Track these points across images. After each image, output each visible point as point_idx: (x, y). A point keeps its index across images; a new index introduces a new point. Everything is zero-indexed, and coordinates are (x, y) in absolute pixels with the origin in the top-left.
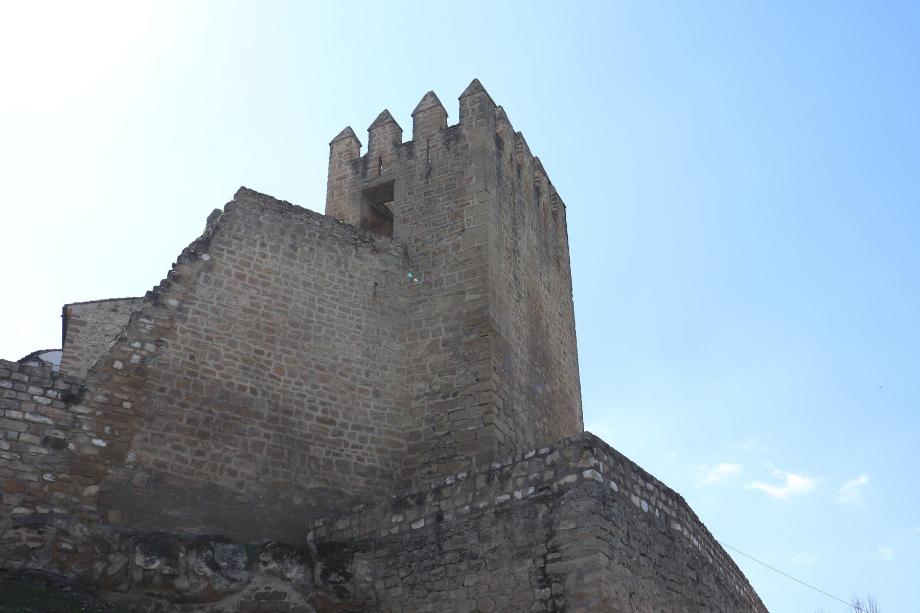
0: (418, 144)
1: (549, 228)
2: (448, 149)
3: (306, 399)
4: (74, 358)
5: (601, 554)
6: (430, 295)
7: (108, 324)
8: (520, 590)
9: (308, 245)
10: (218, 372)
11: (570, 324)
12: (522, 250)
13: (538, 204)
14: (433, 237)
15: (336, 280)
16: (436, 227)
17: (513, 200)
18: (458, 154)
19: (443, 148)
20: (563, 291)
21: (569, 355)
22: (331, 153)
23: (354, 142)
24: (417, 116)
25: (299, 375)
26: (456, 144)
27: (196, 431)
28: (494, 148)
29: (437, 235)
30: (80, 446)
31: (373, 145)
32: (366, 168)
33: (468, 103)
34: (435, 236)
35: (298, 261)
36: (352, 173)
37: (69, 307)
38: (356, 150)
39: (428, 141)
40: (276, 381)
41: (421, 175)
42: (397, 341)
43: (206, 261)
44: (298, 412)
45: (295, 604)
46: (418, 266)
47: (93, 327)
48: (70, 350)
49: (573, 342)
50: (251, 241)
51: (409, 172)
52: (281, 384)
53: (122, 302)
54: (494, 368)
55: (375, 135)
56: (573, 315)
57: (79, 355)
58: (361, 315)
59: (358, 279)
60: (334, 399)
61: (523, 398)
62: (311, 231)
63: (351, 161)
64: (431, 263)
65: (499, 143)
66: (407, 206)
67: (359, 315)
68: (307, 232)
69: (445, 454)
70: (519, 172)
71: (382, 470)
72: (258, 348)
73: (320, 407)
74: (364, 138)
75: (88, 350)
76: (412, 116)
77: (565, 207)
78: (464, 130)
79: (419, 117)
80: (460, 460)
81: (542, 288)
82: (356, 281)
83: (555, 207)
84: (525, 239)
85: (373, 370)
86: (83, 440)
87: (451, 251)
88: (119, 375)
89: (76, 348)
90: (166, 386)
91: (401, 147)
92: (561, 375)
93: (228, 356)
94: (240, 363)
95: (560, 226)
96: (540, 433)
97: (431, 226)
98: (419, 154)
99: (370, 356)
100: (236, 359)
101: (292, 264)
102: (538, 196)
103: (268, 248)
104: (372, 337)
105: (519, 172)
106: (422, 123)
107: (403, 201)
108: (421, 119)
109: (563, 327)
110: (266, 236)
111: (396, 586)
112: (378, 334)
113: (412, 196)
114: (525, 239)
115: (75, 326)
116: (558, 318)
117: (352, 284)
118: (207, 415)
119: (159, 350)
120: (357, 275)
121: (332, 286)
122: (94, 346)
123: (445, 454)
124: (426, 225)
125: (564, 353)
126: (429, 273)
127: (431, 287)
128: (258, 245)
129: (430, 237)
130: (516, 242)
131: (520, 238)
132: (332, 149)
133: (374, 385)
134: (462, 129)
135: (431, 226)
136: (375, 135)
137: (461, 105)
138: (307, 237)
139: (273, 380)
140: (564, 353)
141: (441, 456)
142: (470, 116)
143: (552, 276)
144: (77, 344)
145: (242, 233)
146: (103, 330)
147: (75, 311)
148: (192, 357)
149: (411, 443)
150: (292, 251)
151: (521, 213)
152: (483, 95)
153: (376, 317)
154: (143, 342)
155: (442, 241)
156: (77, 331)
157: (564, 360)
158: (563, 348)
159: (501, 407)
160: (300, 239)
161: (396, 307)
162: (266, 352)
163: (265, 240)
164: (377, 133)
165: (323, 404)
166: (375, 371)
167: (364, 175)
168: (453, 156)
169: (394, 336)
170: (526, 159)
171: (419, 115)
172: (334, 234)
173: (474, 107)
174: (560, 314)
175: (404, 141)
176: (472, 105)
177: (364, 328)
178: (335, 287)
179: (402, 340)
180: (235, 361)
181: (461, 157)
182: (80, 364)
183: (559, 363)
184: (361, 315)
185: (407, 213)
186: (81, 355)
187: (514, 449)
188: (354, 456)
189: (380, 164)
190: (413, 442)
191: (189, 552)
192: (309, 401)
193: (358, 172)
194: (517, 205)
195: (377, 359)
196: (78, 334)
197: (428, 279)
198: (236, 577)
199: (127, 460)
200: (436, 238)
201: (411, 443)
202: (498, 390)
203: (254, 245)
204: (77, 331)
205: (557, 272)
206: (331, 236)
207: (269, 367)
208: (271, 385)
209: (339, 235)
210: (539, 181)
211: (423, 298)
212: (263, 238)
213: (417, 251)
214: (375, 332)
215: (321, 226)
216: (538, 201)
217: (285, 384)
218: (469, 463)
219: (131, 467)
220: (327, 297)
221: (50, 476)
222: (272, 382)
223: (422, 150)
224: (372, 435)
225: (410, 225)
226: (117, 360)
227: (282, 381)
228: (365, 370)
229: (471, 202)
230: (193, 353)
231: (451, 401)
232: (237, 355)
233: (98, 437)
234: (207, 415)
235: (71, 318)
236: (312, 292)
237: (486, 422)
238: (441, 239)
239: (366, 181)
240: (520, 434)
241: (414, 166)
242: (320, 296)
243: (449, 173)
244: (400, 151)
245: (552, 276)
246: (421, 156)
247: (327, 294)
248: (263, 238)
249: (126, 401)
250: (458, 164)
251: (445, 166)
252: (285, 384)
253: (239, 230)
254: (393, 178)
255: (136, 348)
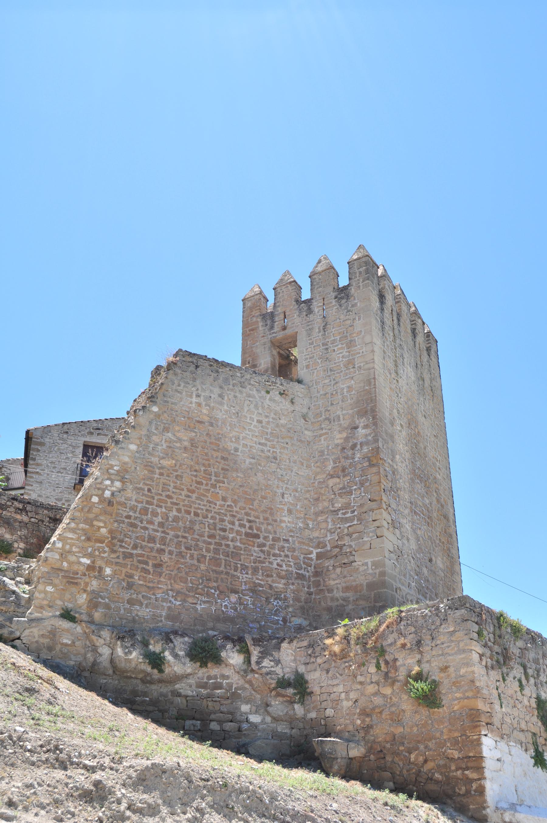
0: (316, 301)
1: (424, 364)
2: (340, 306)
3: (237, 518)
4: (37, 473)
5: (474, 652)
6: (330, 429)
7: (62, 444)
8: (338, 486)
9: (232, 393)
10: (169, 501)
11: (444, 443)
12: (402, 387)
13: (415, 344)
14: (330, 381)
15: (255, 420)
16: (332, 373)
17: (395, 346)
18: (349, 311)
19: (336, 306)
20: (437, 415)
21: (443, 470)
22: (244, 308)
23: (262, 299)
24: (314, 277)
25: (230, 500)
26: (346, 302)
27: (155, 548)
28: (378, 304)
29: (334, 380)
30: (70, 563)
31: (278, 302)
32: (273, 322)
33: (356, 267)
34: (332, 380)
35: (226, 407)
36: (262, 326)
37: (30, 431)
38: (264, 305)
39: (324, 299)
40: (213, 506)
41: (319, 328)
42: (305, 468)
43: (155, 412)
44: (232, 529)
45: (237, 684)
46: (319, 405)
47: (50, 447)
48: (33, 466)
49: (446, 458)
50: (189, 393)
51: (309, 325)
52: (217, 507)
53: (74, 425)
54: (384, 490)
55: (279, 293)
56: (446, 435)
57: (41, 470)
58: (276, 448)
59: (273, 418)
60: (258, 517)
61: (407, 511)
62: (234, 381)
63: (260, 315)
64: (330, 403)
65: (382, 298)
66: (308, 354)
67: (273, 448)
68: (231, 383)
69: (346, 560)
70: (399, 320)
71: (297, 573)
72: (198, 479)
73: (248, 525)
74: (270, 296)
75: (48, 466)
76: (310, 277)
77: (437, 342)
78: (353, 289)
79: (315, 278)
80: (359, 565)
81: (420, 416)
82: (271, 420)
83: (428, 343)
84: (404, 377)
85: (287, 492)
86: (73, 558)
87: (345, 393)
88: (96, 507)
89: (38, 465)
90: (131, 513)
91: (301, 304)
92: (437, 488)
93: (175, 487)
94: (184, 493)
95: (433, 359)
96: (421, 539)
97: (329, 371)
98: (316, 310)
99: (284, 481)
100: (183, 490)
101: (221, 410)
102: (415, 337)
103: (202, 397)
104: (285, 465)
105: (399, 320)
106: (318, 284)
107: (305, 350)
108: (317, 280)
109: (437, 446)
110: (200, 388)
111: (315, 670)
112: (290, 462)
113: (312, 346)
114: (404, 377)
115: (36, 447)
116: (433, 439)
117: (268, 423)
118: (163, 535)
119: (125, 486)
120: (272, 415)
121: (252, 426)
122: (51, 463)
123: (346, 560)
124: (325, 371)
125: (439, 468)
126: (329, 411)
127: (330, 422)
128: (194, 396)
129: (328, 381)
130: (397, 381)
131: (401, 377)
132: (244, 304)
133: (288, 504)
134: (351, 289)
135: (329, 371)
136: (279, 293)
137: (350, 268)
138: (231, 387)
139: (211, 505)
140: (439, 468)
141: (343, 562)
142: (358, 278)
143: (427, 405)
144: (39, 461)
145: (181, 388)
146: (59, 449)
147: (38, 434)
148: (149, 490)
149: (319, 550)
150: (220, 399)
151: (402, 356)
152: (368, 260)
153: (287, 448)
154: (112, 481)
155: (338, 385)
156: (38, 450)
157: (439, 474)
158: (438, 464)
159: (390, 522)
160: (226, 389)
161: (303, 440)
162: (204, 482)
163: (199, 392)
164: (281, 291)
165: (250, 521)
166: (288, 493)
167: (272, 327)
168: (345, 313)
169: (302, 464)
170: (404, 308)
171: (315, 276)
172: (252, 382)
173: (361, 270)
174: (435, 436)
175: (303, 300)
176: (359, 269)
177: (278, 459)
178: (255, 426)
179: (308, 466)
180: (181, 491)
181: (351, 313)
182: (42, 478)
183: (435, 478)
184: (276, 448)
185: (308, 360)
186: (43, 470)
187: (401, 555)
188: (275, 563)
189: (285, 317)
190: (322, 550)
191: (156, 644)
192: (238, 520)
193: (266, 325)
194: (398, 349)
195: (289, 483)
196: (39, 453)
197: (328, 416)
198: (392, 795)
199: (106, 573)
200: (333, 382)
201: (319, 550)
202: (387, 508)
203: (191, 396)
204: (38, 450)
205: (431, 401)
206: (250, 384)
207: (207, 495)
208: (209, 508)
209: (256, 383)
210: (415, 324)
211: (324, 431)
212: (197, 390)
213: (318, 392)
214: (288, 461)
215: (242, 377)
216: (415, 342)
217: (220, 507)
218: (366, 567)
219: (110, 579)
220: (249, 435)
221: (51, 587)
222: (210, 506)
223: (318, 307)
224: (288, 545)
225: (311, 370)
226: (94, 495)
227: (218, 505)
228: (281, 493)
229: (361, 351)
230: (149, 487)
231: (350, 517)
232: (182, 487)
233: (84, 556)
234: (163, 535)
235: (33, 439)
236: (237, 432)
237: (379, 534)
238: (337, 383)
239: (274, 333)
240: (406, 542)
241: (313, 320)
242: (244, 435)
243: (342, 327)
244: (301, 307)
245: (427, 405)
246: (318, 312)
247: (249, 433)
248: (197, 390)
249: (102, 527)
250: (348, 319)
251: (338, 320)
252: (220, 507)
253: (179, 385)
254: (296, 331)
255: (107, 486)
